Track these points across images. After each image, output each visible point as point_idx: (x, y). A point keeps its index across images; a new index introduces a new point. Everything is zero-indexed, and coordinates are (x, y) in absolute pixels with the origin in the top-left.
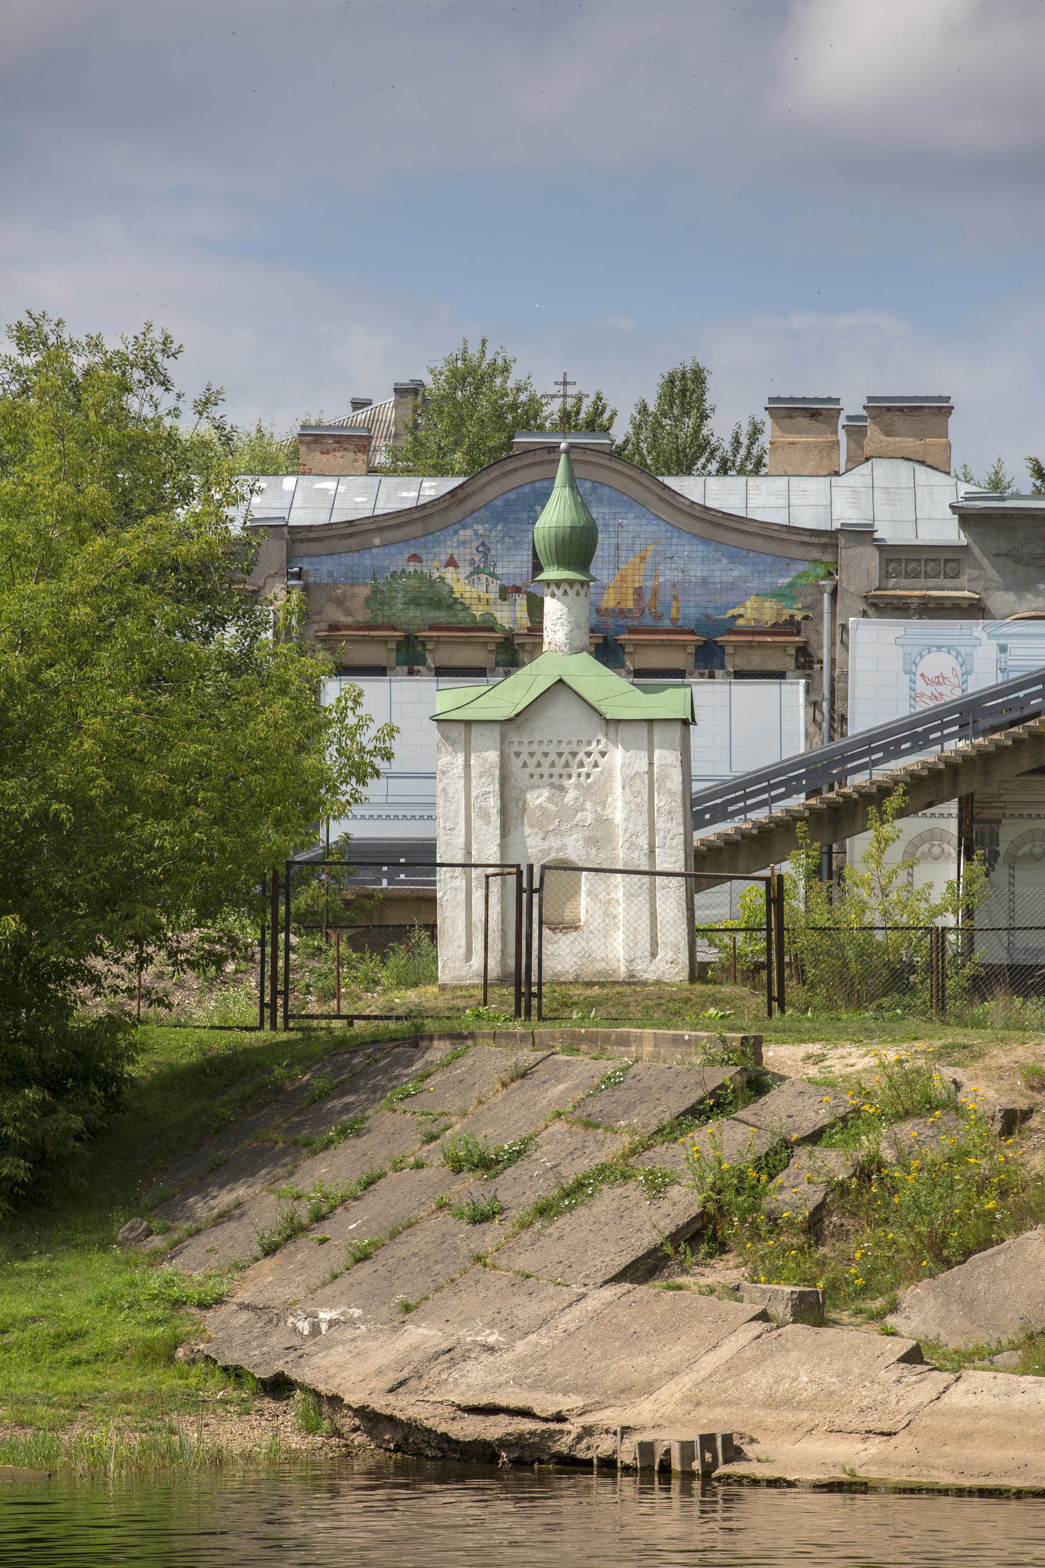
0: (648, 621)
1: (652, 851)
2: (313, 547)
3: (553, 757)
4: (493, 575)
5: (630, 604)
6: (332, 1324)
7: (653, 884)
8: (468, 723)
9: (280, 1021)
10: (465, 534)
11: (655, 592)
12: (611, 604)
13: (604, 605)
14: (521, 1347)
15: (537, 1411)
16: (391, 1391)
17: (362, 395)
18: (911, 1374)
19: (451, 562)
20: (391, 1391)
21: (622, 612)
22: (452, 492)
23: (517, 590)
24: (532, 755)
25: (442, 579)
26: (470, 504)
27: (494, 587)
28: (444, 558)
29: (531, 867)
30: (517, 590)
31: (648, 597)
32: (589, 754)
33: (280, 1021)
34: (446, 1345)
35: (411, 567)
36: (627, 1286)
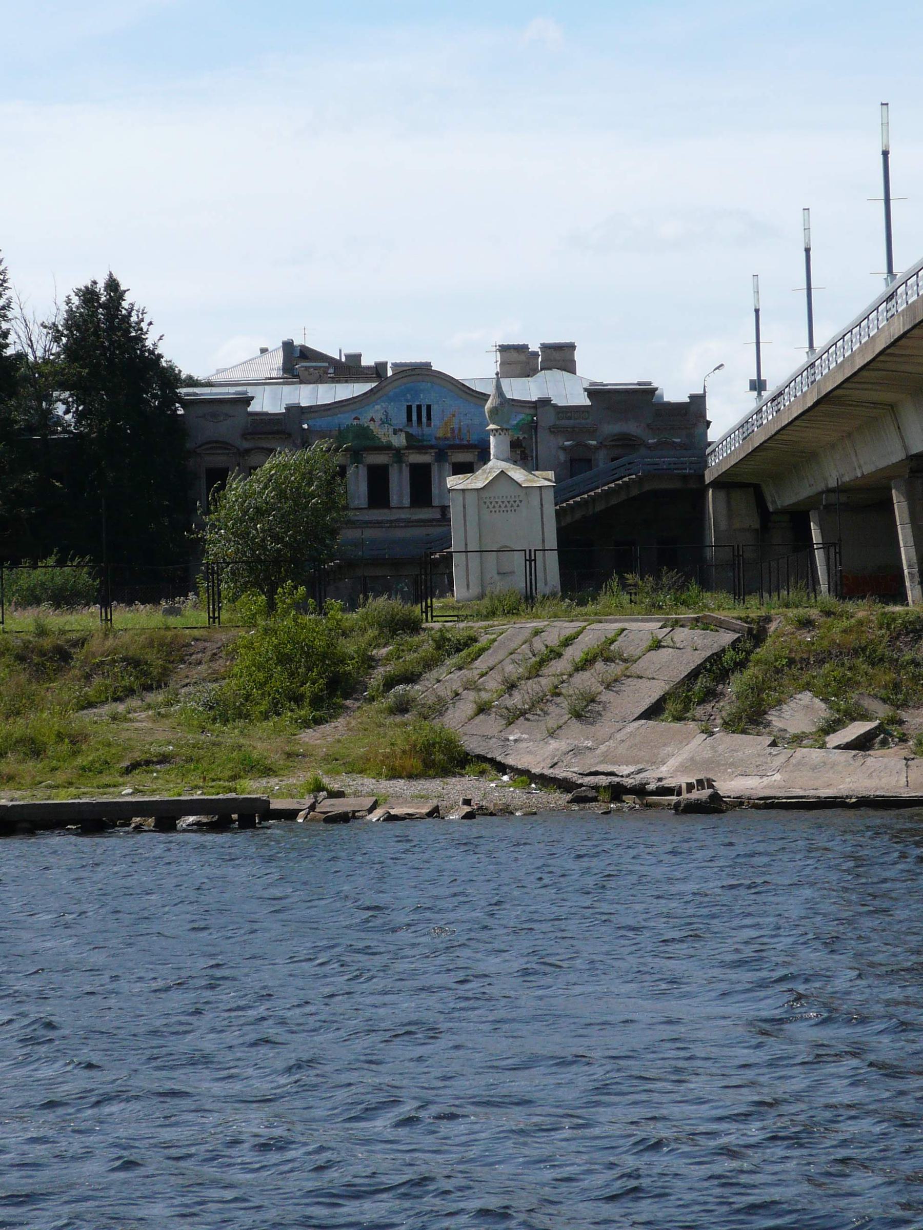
0: (457, 442)
1: (543, 541)
2: (312, 415)
3: (500, 503)
4: (391, 425)
5: (449, 435)
6: (516, 741)
7: (467, 556)
8: (463, 490)
9: (430, 619)
10: (377, 407)
11: (460, 429)
12: (441, 435)
13: (438, 436)
14: (603, 748)
15: (617, 773)
16: (552, 767)
17: (264, 346)
18: (774, 751)
19: (372, 420)
20: (552, 767)
21: (446, 439)
22: (372, 390)
23: (401, 430)
24: (503, 502)
25: (368, 426)
26: (378, 395)
27: (391, 430)
28: (369, 418)
29: (530, 551)
30: (401, 430)
31: (456, 432)
32: (497, 502)
33: (430, 619)
34: (570, 748)
35: (355, 422)
36: (643, 721)
